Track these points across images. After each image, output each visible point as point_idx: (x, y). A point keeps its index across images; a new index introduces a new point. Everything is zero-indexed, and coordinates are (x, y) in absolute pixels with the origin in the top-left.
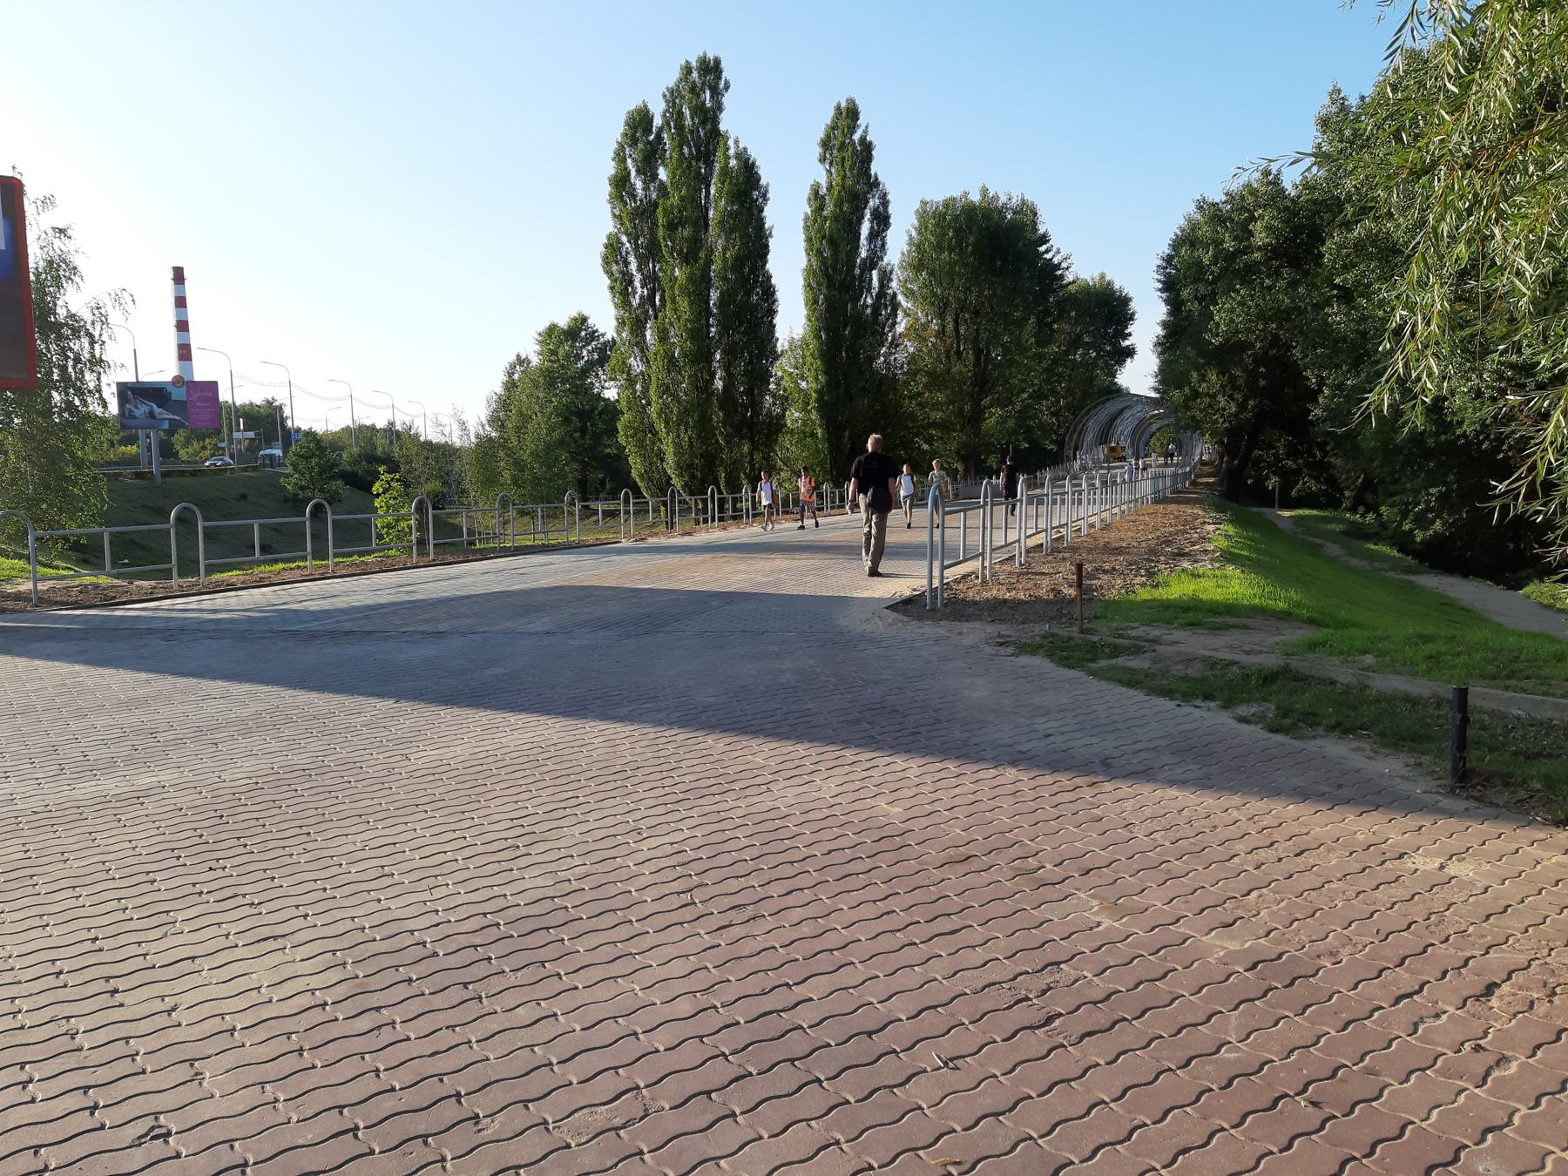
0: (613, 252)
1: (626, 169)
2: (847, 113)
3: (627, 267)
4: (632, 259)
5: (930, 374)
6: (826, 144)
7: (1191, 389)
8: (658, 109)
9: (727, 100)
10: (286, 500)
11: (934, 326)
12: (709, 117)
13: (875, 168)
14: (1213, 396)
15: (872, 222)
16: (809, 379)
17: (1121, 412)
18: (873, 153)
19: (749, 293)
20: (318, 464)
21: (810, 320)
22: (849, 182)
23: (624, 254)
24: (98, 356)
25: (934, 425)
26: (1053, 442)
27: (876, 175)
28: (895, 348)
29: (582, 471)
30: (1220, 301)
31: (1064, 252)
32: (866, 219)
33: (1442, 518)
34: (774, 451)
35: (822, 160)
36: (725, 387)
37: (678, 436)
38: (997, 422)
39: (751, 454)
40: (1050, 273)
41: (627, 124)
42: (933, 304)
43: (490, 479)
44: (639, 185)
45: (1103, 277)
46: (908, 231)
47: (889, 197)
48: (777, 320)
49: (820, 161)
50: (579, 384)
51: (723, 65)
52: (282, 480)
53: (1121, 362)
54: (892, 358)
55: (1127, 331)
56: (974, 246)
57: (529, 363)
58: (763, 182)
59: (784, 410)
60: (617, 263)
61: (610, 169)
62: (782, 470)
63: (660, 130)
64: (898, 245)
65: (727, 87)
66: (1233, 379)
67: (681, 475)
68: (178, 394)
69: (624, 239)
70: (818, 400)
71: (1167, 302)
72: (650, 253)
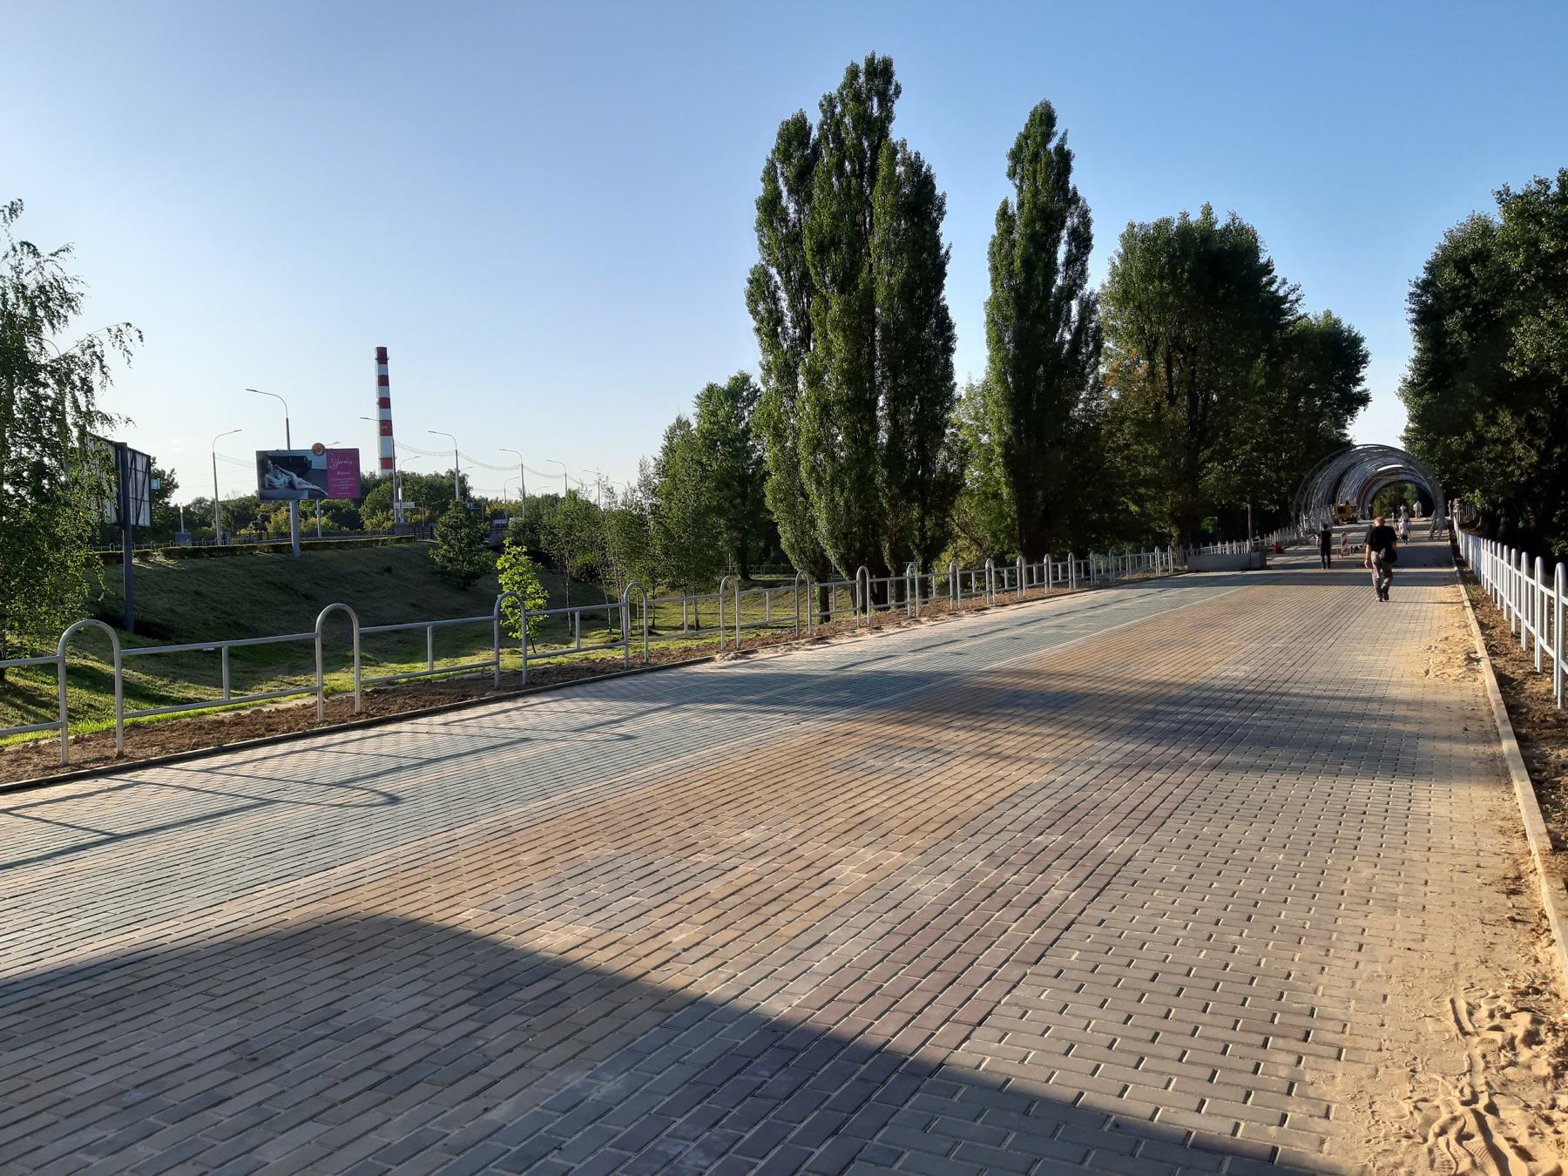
0: (760, 288)
1: (777, 188)
2: (1041, 120)
3: (775, 304)
4: (782, 294)
5: (1141, 423)
6: (1015, 156)
7: (1475, 433)
8: (815, 118)
9: (898, 107)
10: (435, 573)
11: (1142, 369)
12: (877, 128)
13: (1074, 180)
14: (1508, 442)
15: (1069, 244)
16: (992, 431)
17: (1345, 472)
18: (1072, 164)
19: (921, 328)
20: (468, 535)
22: (1042, 198)
23: (772, 288)
24: (84, 409)
25: (1146, 482)
26: (1273, 502)
27: (1075, 188)
28: (1097, 392)
29: (743, 540)
30: (1523, 322)
31: (1291, 283)
32: (1062, 241)
34: (951, 516)
35: (1012, 174)
36: (891, 439)
37: (833, 500)
39: (922, 519)
40: (1276, 305)
41: (780, 136)
42: (1140, 343)
43: (637, 549)
44: (792, 207)
45: (1328, 314)
46: (1110, 259)
47: (1091, 215)
48: (955, 359)
49: (1009, 175)
50: (738, 444)
51: (895, 67)
52: (431, 551)
53: (1351, 411)
55: (1360, 375)
56: (1191, 272)
57: (689, 425)
58: (938, 192)
59: (963, 467)
60: (765, 301)
61: (759, 190)
62: (959, 537)
63: (818, 143)
64: (1099, 274)
65: (898, 92)
66: (1531, 421)
67: (835, 546)
68: (318, 463)
69: (773, 271)
71: (1421, 336)
72: (802, 287)
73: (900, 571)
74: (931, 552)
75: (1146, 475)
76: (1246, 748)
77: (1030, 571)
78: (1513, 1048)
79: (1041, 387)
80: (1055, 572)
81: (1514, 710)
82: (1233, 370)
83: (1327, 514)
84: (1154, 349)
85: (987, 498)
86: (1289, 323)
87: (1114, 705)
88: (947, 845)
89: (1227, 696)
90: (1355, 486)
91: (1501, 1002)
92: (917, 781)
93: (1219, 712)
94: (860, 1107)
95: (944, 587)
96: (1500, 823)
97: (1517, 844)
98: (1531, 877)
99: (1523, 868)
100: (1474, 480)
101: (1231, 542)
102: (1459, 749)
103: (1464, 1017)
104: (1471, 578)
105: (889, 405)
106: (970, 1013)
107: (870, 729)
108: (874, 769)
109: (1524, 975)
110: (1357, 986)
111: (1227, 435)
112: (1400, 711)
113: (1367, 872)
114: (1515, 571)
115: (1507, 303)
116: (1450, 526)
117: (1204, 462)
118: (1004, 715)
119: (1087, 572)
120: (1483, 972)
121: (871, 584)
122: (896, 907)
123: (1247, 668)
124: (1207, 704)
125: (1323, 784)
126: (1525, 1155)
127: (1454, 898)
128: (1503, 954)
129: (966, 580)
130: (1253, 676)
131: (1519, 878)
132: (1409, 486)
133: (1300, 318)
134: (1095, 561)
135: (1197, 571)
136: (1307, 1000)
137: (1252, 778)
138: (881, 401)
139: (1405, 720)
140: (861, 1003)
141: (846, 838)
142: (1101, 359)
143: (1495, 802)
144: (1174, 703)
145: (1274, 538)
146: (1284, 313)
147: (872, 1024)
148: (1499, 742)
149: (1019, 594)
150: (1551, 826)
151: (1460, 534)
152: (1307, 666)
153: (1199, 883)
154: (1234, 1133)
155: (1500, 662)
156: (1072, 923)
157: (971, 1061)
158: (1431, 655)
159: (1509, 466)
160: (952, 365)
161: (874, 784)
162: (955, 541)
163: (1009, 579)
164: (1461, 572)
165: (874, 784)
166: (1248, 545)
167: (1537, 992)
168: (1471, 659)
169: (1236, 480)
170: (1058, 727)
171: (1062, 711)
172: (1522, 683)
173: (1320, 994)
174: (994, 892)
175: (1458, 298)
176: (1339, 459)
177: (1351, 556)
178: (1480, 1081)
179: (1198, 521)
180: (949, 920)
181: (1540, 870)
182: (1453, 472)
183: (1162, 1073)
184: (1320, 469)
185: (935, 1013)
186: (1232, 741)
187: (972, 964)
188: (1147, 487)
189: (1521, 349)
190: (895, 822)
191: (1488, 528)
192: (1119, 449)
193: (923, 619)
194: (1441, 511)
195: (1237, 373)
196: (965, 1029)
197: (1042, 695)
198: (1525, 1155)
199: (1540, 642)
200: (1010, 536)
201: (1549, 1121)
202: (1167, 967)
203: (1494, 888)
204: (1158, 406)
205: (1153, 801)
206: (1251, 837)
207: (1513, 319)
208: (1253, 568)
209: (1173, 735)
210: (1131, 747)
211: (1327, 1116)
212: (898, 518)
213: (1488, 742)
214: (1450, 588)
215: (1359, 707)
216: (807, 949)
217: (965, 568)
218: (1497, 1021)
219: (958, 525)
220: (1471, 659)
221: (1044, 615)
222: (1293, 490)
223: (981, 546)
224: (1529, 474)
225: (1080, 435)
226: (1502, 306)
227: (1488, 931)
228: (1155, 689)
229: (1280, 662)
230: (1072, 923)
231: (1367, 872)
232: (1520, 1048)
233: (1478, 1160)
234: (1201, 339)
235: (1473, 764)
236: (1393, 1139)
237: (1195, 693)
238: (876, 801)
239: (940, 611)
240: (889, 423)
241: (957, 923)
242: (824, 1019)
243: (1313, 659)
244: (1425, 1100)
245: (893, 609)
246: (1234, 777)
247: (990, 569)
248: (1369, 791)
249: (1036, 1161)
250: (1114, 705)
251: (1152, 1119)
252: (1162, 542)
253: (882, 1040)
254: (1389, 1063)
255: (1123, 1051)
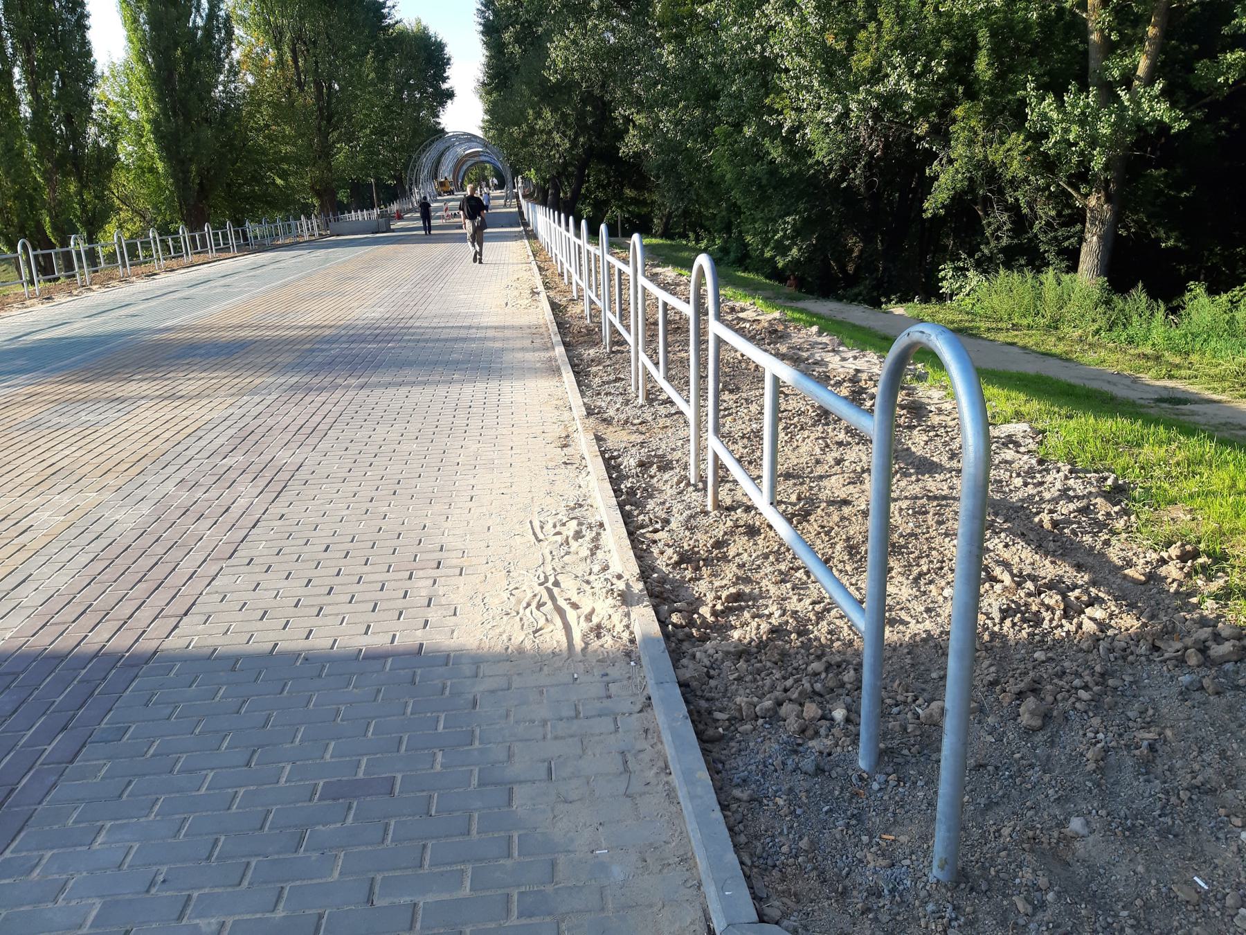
5: (276, 105)
11: (271, 57)
14: (550, 132)
17: (442, 154)
21: (131, 42)
25: (286, 159)
26: (393, 177)
30: (555, 39)
33: (796, 244)
34: (110, 189)
38: (346, 157)
48: (90, 35)
53: (442, 104)
54: (232, 86)
59: (115, 142)
66: (564, 115)
70: (156, 130)
71: (488, 45)
73: (65, 243)
74: (94, 224)
75: (286, 153)
76: (385, 370)
77: (193, 239)
78: (568, 544)
79: (181, 68)
80: (217, 240)
81: (561, 326)
82: (350, 64)
83: (431, 188)
84: (280, 41)
85: (143, 172)
86: (389, 26)
87: (279, 347)
88: (141, 479)
89: (368, 332)
90: (451, 165)
91: (560, 517)
92: (106, 430)
93: (362, 345)
94: (85, 702)
95: (111, 258)
96: (555, 402)
97: (566, 415)
98: (575, 434)
99: (570, 429)
100: (531, 161)
101: (362, 211)
102: (529, 356)
103: (538, 530)
104: (532, 235)
105: (26, 79)
106: (179, 607)
107: (51, 389)
108: (61, 425)
109: (572, 496)
110: (471, 525)
111: (349, 120)
112: (491, 333)
113: (474, 447)
114: (558, 227)
115: (544, 23)
116: (517, 197)
117: (334, 142)
118: (183, 365)
119: (246, 239)
120: (549, 500)
121: (36, 257)
122: (97, 538)
123: (381, 309)
124: (353, 339)
125: (441, 390)
126: (575, 606)
127: (530, 455)
128: (560, 487)
129: (132, 249)
130: (387, 316)
131: (568, 436)
132: (488, 166)
133: (397, 23)
134: (251, 228)
135: (338, 235)
136: (438, 541)
137: (391, 391)
138: (17, 72)
139: (494, 339)
140: (74, 622)
141: (39, 489)
142: (234, 45)
143: (552, 389)
144: (328, 342)
145: (395, 207)
146: (384, 17)
147: (86, 636)
148: (553, 348)
149: (185, 260)
150: (585, 400)
151: (523, 202)
152: (426, 305)
153: (356, 474)
154: (392, 642)
155: (552, 294)
156: (258, 521)
157: (182, 643)
158: (509, 292)
159: (551, 150)
160: (89, 43)
161: (62, 438)
162: (118, 213)
163: (174, 247)
164: (525, 230)
165: (62, 438)
166: (376, 212)
167: (581, 506)
168: (534, 293)
169: (360, 158)
170: (233, 370)
171: (236, 356)
172: (566, 307)
173: (446, 534)
174: (188, 510)
175: (511, 17)
176: (436, 143)
177: (452, 220)
178: (549, 571)
179: (334, 194)
180: (147, 540)
181: (580, 429)
182: (516, 155)
183: (338, 614)
184: (424, 151)
185: (145, 614)
186: (375, 366)
187: (174, 569)
188: (289, 164)
189: (554, 60)
190: (88, 468)
191: (542, 197)
192: (259, 130)
193: (94, 287)
194: (510, 185)
195: (352, 67)
196: (174, 621)
197: (215, 345)
198: (575, 606)
199: (575, 277)
200: (170, 207)
201: (588, 582)
202: (336, 539)
203: (553, 445)
204: (289, 90)
205: (317, 419)
206: (394, 436)
207: (548, 36)
208: (381, 231)
209: (330, 365)
210: (295, 379)
211: (455, 614)
212: (55, 192)
213: (547, 349)
214: (519, 242)
215: (463, 333)
216: (13, 590)
217: (131, 238)
218: (558, 529)
219: (118, 198)
220: (534, 293)
221: (211, 277)
222: (406, 167)
223: (144, 218)
224: (565, 157)
225: (224, 114)
226: (541, 26)
227: (551, 472)
228: (312, 332)
229: (407, 303)
230: (258, 521)
231: (474, 447)
232: (571, 541)
233: (549, 617)
234: (319, 34)
235: (538, 365)
236: (498, 618)
237: (343, 332)
238: (67, 452)
239: (111, 278)
240: (29, 97)
241: (157, 541)
242: (42, 641)
243: (430, 300)
244: (517, 588)
245: (62, 279)
246: (378, 392)
247: (154, 238)
248: (472, 391)
249: (244, 702)
250: (279, 347)
251: (332, 648)
252: (306, 210)
253: (97, 647)
254: (493, 570)
255: (306, 606)
